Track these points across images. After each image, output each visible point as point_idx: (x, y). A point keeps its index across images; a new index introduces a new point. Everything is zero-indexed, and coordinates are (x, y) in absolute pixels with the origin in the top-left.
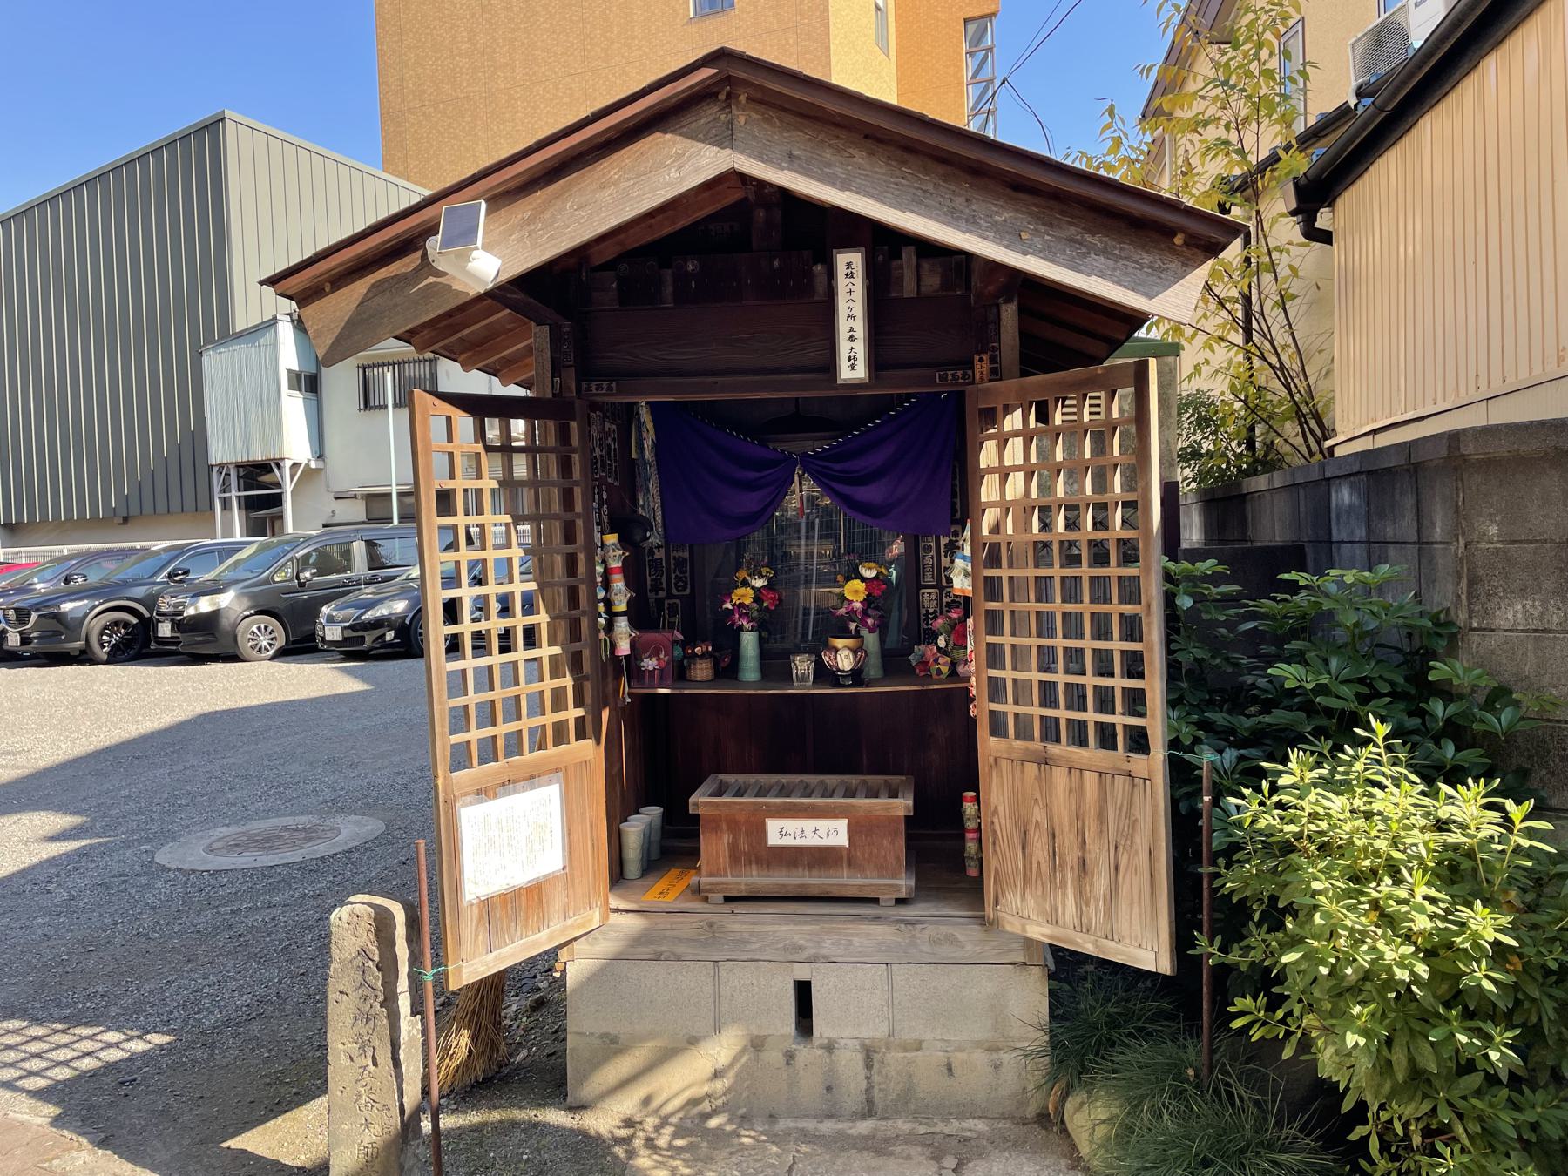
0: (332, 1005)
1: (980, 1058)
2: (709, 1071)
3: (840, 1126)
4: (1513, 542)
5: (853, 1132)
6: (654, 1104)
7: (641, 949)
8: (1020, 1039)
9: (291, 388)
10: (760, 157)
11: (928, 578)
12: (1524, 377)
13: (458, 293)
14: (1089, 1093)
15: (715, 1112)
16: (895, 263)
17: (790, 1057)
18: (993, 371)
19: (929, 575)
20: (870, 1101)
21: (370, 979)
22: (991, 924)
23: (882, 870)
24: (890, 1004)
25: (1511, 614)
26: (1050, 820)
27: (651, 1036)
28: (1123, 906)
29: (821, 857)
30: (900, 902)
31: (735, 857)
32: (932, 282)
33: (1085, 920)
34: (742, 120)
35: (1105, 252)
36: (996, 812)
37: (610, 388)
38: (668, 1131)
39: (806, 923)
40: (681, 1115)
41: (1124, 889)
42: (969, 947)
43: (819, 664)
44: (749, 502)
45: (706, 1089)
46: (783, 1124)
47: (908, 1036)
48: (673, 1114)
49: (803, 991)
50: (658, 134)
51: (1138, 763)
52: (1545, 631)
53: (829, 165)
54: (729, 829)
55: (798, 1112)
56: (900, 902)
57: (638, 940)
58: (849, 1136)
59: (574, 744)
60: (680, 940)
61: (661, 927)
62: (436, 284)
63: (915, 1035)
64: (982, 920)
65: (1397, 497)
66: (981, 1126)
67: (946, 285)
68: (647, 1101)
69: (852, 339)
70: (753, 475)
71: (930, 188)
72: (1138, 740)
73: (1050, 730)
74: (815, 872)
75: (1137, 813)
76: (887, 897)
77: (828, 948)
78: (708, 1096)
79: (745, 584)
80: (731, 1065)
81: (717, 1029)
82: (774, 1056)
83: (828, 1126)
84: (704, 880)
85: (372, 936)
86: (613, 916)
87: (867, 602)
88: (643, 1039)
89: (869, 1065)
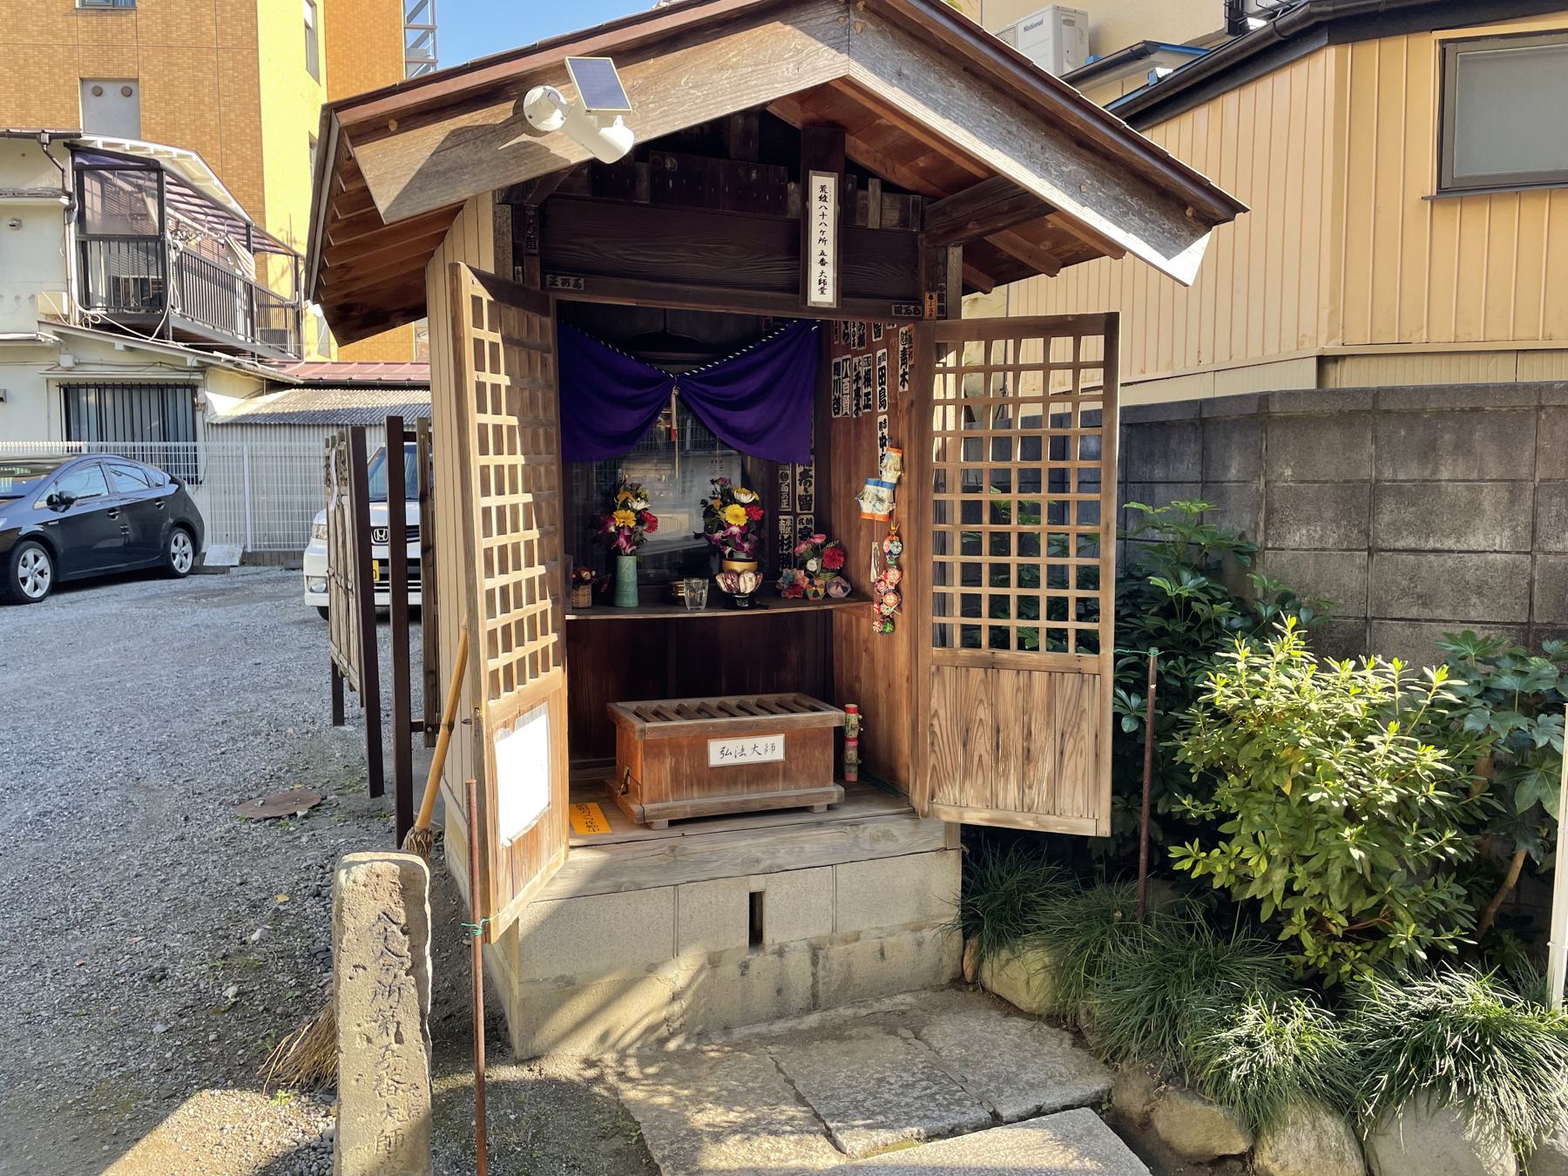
0: (345, 983)
1: (908, 938)
2: (668, 994)
3: (790, 1024)
4: (1302, 482)
5: (803, 1027)
6: (611, 1040)
7: (601, 883)
8: (940, 916)
9: (1168, 257)
10: (873, 69)
11: (784, 506)
12: (1255, 355)
13: (557, 158)
14: (1013, 952)
15: (672, 1035)
16: (861, 193)
17: (745, 967)
18: (941, 309)
19: (785, 501)
20: (815, 996)
21: (395, 946)
22: (925, 816)
23: (813, 779)
24: (835, 902)
25: (1298, 536)
26: (995, 717)
27: (610, 970)
28: (1066, 786)
29: (759, 773)
30: (830, 808)
31: (677, 779)
32: (892, 217)
33: (1027, 800)
34: (859, 27)
35: (1139, 214)
36: (936, 714)
37: (577, 285)
38: (631, 1062)
39: (760, 836)
40: (639, 1044)
41: (1068, 770)
42: (902, 840)
43: (714, 587)
44: (630, 419)
45: (664, 1013)
46: (739, 1033)
47: (847, 929)
48: (630, 1045)
49: (755, 900)
50: (778, 23)
51: (1089, 661)
52: (1324, 549)
53: (932, 90)
54: (673, 753)
55: (749, 1019)
56: (830, 808)
57: (599, 874)
58: (803, 1031)
59: (543, 675)
60: (642, 868)
61: (623, 857)
62: (527, 145)
63: (855, 928)
64: (913, 813)
65: (1173, 445)
66: (909, 999)
67: (904, 221)
68: (604, 1038)
69: (823, 262)
70: (629, 392)
71: (1014, 129)
72: (1089, 642)
73: (1000, 639)
74: (753, 788)
75: (1086, 704)
76: (820, 805)
77: (783, 858)
78: (666, 1020)
79: (625, 506)
80: (689, 985)
81: (676, 953)
82: (730, 970)
83: (779, 1027)
84: (648, 807)
85: (396, 897)
86: (572, 852)
87: (745, 529)
88: (600, 975)
89: (815, 963)
